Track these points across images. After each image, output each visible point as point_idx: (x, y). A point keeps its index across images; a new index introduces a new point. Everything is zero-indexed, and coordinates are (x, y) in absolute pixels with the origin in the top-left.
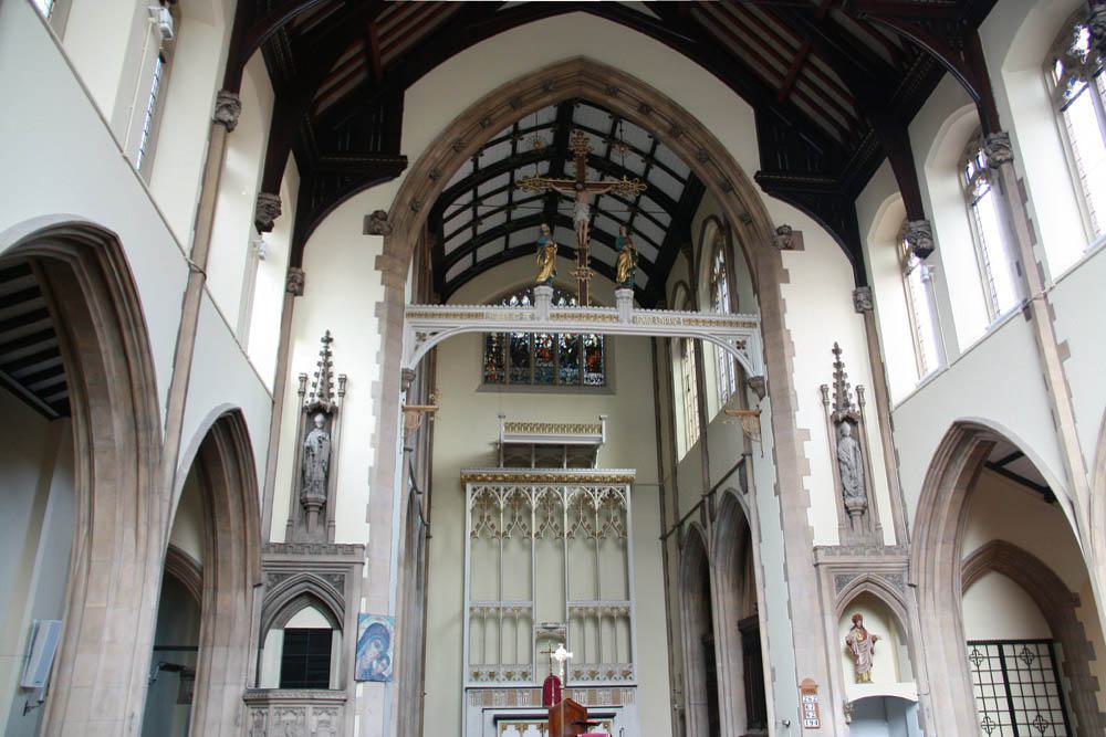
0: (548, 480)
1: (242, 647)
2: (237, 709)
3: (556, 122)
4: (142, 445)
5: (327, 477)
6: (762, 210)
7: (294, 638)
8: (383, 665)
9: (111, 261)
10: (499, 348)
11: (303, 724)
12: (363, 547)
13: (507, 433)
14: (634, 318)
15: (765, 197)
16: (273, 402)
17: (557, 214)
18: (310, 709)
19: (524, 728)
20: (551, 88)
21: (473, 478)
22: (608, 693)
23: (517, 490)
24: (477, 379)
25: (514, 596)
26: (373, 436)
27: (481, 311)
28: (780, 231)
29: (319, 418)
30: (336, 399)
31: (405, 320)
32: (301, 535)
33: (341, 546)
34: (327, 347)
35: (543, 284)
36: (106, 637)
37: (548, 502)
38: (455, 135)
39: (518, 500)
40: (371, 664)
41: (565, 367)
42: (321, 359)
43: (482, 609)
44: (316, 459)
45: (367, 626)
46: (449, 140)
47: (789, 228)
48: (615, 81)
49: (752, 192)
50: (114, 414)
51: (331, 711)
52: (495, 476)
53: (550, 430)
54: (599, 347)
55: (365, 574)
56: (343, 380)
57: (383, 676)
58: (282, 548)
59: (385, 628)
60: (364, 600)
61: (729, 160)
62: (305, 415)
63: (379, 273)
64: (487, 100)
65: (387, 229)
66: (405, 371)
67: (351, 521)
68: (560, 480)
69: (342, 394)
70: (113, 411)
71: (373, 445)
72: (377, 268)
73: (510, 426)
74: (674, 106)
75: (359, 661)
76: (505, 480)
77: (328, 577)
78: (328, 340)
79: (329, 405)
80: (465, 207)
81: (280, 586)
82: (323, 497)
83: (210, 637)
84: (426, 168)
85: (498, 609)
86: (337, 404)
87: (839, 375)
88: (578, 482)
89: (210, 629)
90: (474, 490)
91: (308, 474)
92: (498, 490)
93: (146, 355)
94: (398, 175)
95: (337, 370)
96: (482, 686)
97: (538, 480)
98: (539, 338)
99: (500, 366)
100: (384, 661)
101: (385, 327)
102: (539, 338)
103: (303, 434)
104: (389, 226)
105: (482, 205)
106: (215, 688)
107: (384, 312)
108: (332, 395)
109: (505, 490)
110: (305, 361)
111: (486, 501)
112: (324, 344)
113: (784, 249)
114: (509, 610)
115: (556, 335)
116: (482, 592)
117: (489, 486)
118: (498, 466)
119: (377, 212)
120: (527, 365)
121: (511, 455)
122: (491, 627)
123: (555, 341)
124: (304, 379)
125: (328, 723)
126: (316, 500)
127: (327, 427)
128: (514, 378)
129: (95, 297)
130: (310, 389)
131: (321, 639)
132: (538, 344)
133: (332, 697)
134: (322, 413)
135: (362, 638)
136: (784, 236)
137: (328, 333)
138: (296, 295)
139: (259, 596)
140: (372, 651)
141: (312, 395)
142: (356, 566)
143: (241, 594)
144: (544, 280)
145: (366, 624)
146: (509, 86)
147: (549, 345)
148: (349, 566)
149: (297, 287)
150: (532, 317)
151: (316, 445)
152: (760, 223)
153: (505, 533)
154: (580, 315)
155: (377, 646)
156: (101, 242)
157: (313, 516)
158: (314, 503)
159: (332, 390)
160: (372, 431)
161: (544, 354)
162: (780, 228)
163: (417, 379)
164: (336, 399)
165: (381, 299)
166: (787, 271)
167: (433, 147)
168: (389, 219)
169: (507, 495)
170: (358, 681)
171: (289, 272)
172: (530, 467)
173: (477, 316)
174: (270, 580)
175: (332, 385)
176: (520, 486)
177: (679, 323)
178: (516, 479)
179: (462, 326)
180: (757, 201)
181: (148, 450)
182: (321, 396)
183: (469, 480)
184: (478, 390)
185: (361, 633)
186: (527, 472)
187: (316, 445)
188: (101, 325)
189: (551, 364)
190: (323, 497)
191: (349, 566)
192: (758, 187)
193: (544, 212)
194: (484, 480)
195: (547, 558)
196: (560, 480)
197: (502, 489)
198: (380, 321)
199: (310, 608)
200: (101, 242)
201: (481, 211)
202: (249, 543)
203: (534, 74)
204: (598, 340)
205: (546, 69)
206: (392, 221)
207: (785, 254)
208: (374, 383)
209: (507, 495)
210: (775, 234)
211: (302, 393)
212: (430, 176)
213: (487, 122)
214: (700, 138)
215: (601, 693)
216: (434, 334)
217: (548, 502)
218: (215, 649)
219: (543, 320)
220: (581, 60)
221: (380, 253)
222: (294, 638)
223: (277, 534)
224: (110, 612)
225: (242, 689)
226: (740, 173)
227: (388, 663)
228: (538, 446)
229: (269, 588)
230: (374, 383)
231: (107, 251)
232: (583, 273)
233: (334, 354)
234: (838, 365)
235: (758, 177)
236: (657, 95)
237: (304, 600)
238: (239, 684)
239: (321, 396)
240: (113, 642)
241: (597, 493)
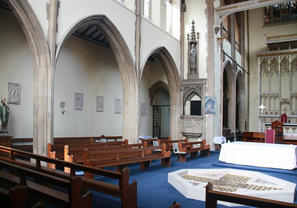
0: (284, 54)
1: (179, 105)
2: (179, 120)
4: (129, 61)
5: (196, 60)
7: (192, 103)
8: (213, 110)
9: (106, 21)
11: (192, 123)
12: (206, 79)
13: (267, 41)
16: (181, 43)
18: (193, 120)
19: (294, 129)
21: (259, 56)
22: (270, 119)
23: (274, 58)
24: (262, 24)
25: (275, 90)
26: (207, 48)
27: (237, 5)
29: (193, 45)
30: (197, 40)
31: (215, 13)
32: (192, 77)
33: (200, 79)
34: (193, 25)
36: (129, 103)
37: (284, 61)
39: (274, 61)
40: (209, 109)
41: (293, 14)
42: (192, 29)
43: (263, 94)
44: (193, 56)
45: (207, 100)
50: (121, 55)
51: (191, 120)
52: (266, 54)
53: (284, 37)
55: (207, 86)
56: (198, 34)
57: (213, 112)
58: (186, 81)
59: (213, 100)
60: (207, 93)
62: (189, 45)
66: (216, 28)
67: (203, 73)
68: (288, 53)
69: (198, 38)
70: (120, 54)
71: (207, 51)
73: (268, 38)
75: (206, 109)
76: (270, 55)
77: (198, 87)
78: (193, 23)
79: (194, 41)
81: (187, 90)
82: (195, 67)
83: (172, 103)
85: (268, 94)
86: (197, 41)
87: (193, 30)
88: (294, 53)
89: (172, 101)
90: (260, 59)
91: (191, 61)
92: (268, 58)
93: (123, 40)
95: (196, 31)
96: (295, 116)
97: (281, 54)
98: (283, 6)
99: (270, 18)
100: (213, 109)
101: (208, 16)
103: (189, 50)
106: (174, 115)
108: (195, 38)
109: (270, 58)
110: (188, 30)
111: (264, 62)
112: (192, 24)
114: (272, 95)
115: (290, 3)
116: (265, 90)
117: (265, 57)
118: (267, 51)
120: (279, 16)
121: (272, 47)
122: (273, 100)
123: (289, 5)
124: (188, 35)
125: (198, 124)
126: (194, 67)
127: (195, 47)
128: (275, 21)
129: (107, 29)
130: (190, 38)
131: (199, 103)
132: (283, 8)
133: (199, 117)
134: (193, 44)
135: (206, 103)
137: (193, 21)
138: (184, 12)
139: (182, 92)
140: (209, 106)
141: (190, 39)
142: (204, 84)
143: (177, 93)
145: (207, 99)
147: (287, 7)
148: (202, 84)
149: (184, 10)
150: (253, 4)
151: (192, 53)
153: (270, 72)
155: (211, 105)
156: (102, 18)
157: (194, 72)
158: (193, 69)
159: (195, 37)
160: (206, 46)
161: (284, 11)
163: (220, 30)
164: (197, 40)
165: (206, 8)
169: (281, 59)
170: (206, 114)
171: (181, 6)
172: (289, 49)
173: (236, 7)
174: (184, 89)
175: (195, 36)
176: (275, 57)
178: (273, 54)
179: (232, 11)
181: (130, 62)
182: (192, 39)
183: (259, 56)
184: (263, 27)
185: (206, 101)
186: (277, 52)
187: (192, 53)
188: (111, 36)
189: (288, 14)
190: (195, 67)
191: (202, 84)
194: (263, 56)
195: (286, 78)
196: (288, 53)
197: (279, 57)
198: (206, 15)
199: (196, 95)
200: (102, 18)
202: (177, 80)
208: (206, 33)
209: (271, 59)
211: (188, 39)
215: (267, 119)
216: (223, 15)
217: (284, 61)
218: (173, 106)
219: (256, 4)
222: (192, 103)
223: (186, 78)
224: (129, 98)
225: (180, 115)
227: (214, 109)
228: (280, 43)
229: (184, 91)
230: (206, 33)
231: (104, 19)
233: (195, 27)
234: (193, 27)
237: (194, 94)
238: (179, 114)
239: (192, 39)
240: (130, 104)
241: (269, 59)
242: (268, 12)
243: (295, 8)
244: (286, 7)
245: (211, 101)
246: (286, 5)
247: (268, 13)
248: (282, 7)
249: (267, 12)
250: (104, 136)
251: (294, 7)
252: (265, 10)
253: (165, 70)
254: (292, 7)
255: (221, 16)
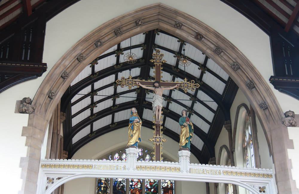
3: (144, 44)
6: (274, 101)
10: (106, 188)
14: (190, 169)
15: (277, 93)
17: (145, 101)
20: (140, 23)
27: (232, 170)
28: (286, 115)
31: (41, 170)
35: (132, 146)
38: (78, 52)
46: (75, 54)
47: (293, 112)
48: (180, 19)
49: (268, 90)
54: (172, 187)
61: (252, 68)
63: (25, 138)
64: (100, 29)
65: (31, 109)
72: (26, 145)
74: (218, 36)
80: (86, 96)
84: (59, 71)
94: (40, 75)
101: (25, 174)
102: (132, 181)
104: (33, 108)
105: (96, 95)
107: (26, 164)
113: (289, 126)
119: (25, 99)
132: (131, 186)
136: (289, 118)
144: (132, 144)
146: (114, 21)
150: (124, 168)
152: (273, 109)
154: (232, 172)
162: (286, 112)
166: (292, 141)
167: (64, 58)
168: (33, 104)
173: (88, 167)
177: (220, 173)
180: (271, 95)
192: (272, 86)
193: (136, 100)
201: (96, 98)
203: (129, 15)
204: (171, 183)
205: (137, 12)
206: (35, 104)
207: (290, 129)
210: (284, 116)
212: (62, 76)
213: (99, 44)
214: (234, 56)
216: (59, 178)
219: (131, 170)
220: (159, 6)
221: (26, 125)
226: (259, 77)
232: (158, 140)
235: (272, 80)
236: (207, 28)
242: (104, 187)
243: (152, 190)
244: (137, 184)
245: (188, 37)
246: (138, 182)
247: (102, 189)
248: (131, 184)
249: (101, 187)
250: (272, 77)
251: (151, 189)
252: (98, 183)
253: (52, 74)
254: (147, 188)
255: (53, 179)
